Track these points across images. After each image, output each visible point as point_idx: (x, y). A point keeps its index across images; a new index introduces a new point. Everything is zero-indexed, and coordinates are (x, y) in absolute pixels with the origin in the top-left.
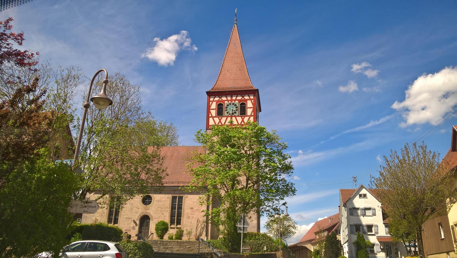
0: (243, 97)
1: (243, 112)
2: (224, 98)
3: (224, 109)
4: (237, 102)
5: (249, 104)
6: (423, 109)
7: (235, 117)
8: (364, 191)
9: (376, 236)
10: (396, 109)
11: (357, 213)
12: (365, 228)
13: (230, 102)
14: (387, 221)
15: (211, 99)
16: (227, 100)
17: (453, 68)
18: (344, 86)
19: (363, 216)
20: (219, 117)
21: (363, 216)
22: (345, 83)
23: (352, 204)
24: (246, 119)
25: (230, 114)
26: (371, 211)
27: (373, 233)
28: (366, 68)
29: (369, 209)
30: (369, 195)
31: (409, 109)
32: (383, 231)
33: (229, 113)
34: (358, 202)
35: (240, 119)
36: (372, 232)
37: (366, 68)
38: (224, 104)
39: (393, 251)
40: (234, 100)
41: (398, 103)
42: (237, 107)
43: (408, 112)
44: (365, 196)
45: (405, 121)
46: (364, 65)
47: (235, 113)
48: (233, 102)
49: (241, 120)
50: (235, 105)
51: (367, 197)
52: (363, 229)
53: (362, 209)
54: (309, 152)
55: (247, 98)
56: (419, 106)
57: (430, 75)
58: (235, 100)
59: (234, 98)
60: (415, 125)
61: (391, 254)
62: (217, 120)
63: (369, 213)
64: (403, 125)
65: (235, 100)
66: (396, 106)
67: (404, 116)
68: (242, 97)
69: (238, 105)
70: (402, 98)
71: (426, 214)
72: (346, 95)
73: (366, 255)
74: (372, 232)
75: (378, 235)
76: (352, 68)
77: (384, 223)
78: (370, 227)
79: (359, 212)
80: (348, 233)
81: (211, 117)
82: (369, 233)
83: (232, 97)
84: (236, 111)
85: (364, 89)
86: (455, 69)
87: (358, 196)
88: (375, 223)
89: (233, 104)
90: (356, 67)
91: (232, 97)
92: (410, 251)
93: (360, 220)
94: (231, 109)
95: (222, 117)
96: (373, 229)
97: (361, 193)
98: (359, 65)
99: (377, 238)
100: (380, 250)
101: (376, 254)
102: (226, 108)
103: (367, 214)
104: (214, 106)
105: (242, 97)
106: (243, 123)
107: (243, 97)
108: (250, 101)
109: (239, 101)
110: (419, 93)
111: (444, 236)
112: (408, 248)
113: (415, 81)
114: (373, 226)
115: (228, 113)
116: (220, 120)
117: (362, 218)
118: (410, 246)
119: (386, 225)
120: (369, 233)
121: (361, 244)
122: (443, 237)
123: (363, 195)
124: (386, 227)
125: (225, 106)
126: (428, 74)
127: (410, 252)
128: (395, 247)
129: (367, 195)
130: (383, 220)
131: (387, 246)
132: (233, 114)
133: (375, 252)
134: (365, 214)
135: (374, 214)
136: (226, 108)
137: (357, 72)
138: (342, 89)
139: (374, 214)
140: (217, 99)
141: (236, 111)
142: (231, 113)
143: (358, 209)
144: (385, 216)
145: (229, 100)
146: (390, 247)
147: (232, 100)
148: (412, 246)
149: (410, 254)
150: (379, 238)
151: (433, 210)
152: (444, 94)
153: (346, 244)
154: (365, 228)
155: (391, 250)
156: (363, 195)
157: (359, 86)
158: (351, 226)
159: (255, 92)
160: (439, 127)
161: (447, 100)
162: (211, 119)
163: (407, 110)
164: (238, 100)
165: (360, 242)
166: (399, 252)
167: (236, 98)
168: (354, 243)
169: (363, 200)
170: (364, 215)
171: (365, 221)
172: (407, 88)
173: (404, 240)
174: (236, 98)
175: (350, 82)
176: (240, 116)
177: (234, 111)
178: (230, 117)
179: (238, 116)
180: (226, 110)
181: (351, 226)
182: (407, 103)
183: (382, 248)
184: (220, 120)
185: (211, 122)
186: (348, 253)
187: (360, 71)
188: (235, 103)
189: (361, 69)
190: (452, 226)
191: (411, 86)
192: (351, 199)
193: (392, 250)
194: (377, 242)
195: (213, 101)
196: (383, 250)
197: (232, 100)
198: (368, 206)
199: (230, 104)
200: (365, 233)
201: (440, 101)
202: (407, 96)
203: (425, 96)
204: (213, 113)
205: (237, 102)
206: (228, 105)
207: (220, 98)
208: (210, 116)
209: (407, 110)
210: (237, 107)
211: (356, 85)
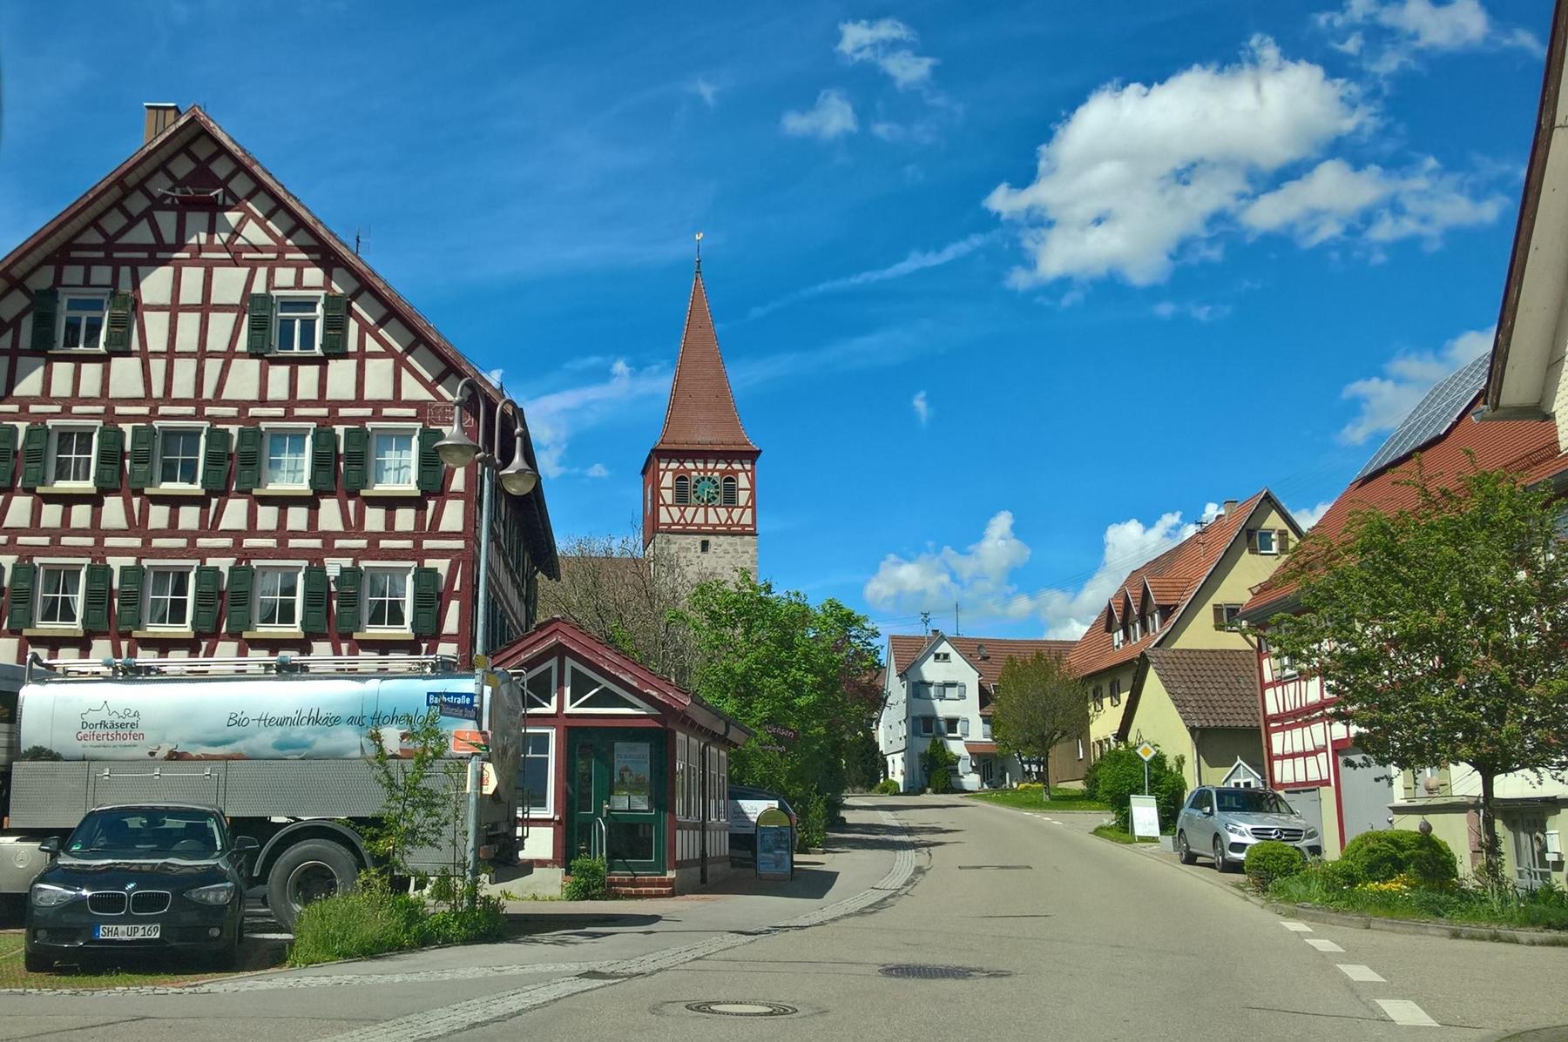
0: (730, 464)
1: (730, 500)
2: (690, 466)
3: (690, 489)
4: (716, 474)
5: (743, 481)
6: (1098, 221)
7: (715, 507)
8: (944, 648)
9: (962, 742)
10: (998, 214)
11: (928, 692)
12: (943, 725)
13: (702, 473)
14: (989, 710)
15: (663, 466)
16: (696, 469)
17: (1220, 70)
18: (803, 112)
19: (941, 700)
20: (679, 507)
21: (941, 700)
22: (807, 100)
23: (920, 674)
24: (736, 513)
25: (703, 501)
26: (957, 688)
27: (958, 734)
28: (893, 46)
29: (953, 685)
30: (954, 655)
31: (1051, 215)
32: (977, 731)
33: (701, 499)
34: (932, 671)
35: (723, 512)
36: (956, 732)
37: (893, 46)
38: (690, 478)
39: (996, 771)
40: (710, 470)
41: (1014, 190)
42: (717, 487)
43: (1043, 232)
44: (946, 656)
45: (1030, 264)
46: (887, 30)
47: (714, 498)
48: (709, 474)
49: (727, 515)
50: (714, 482)
51: (951, 660)
52: (938, 727)
53: (939, 685)
54: (655, 368)
55: (737, 466)
56: (1084, 210)
57: (1134, 88)
58: (714, 470)
59: (710, 466)
60: (1063, 283)
61: (991, 777)
62: (675, 512)
63: (951, 692)
64: (1020, 279)
65: (714, 470)
66: (1002, 200)
67: (1028, 244)
68: (726, 465)
69: (719, 483)
70: (1025, 177)
71: (1056, 737)
72: (810, 147)
73: (946, 779)
74: (956, 732)
75: (968, 739)
76: (838, 37)
77: (981, 716)
78: (952, 723)
79: (932, 690)
80: (907, 732)
81: (662, 505)
82: (950, 735)
83: (706, 463)
84: (716, 496)
85: (881, 129)
86: (1226, 74)
87: (932, 657)
88: (962, 715)
89: (709, 479)
90: (855, 36)
91: (706, 463)
92: (1030, 772)
93: (933, 709)
94: (706, 490)
95: (686, 507)
96: (958, 725)
97: (937, 651)
98: (870, 27)
99: (966, 745)
100: (970, 769)
101: (962, 777)
102: (695, 487)
103: (947, 696)
104: (668, 480)
105: (726, 465)
106: (730, 522)
107: (730, 464)
108: (744, 474)
109: (722, 472)
110: (1094, 158)
111: (1083, 755)
112: (1026, 767)
113: (1081, 111)
114: (958, 719)
115: (698, 498)
116: (682, 513)
117: (936, 702)
118: (1029, 763)
119: (986, 719)
120: (950, 735)
121: (939, 759)
122: (1081, 757)
123: (942, 656)
124: (984, 722)
125: (693, 482)
126: (1125, 84)
127: (1029, 775)
128: (999, 765)
129: (951, 655)
130: (980, 709)
131: (984, 761)
132: (709, 501)
133: (961, 773)
134: (944, 696)
135: (962, 697)
136: (695, 487)
137: (858, 57)
138: (795, 123)
139: (962, 697)
140: (674, 465)
141: (716, 496)
142: (705, 499)
143: (931, 684)
144: (985, 698)
145: (701, 470)
146: (991, 763)
147: (705, 470)
148: (1034, 763)
149: (1029, 778)
150: (969, 745)
151: (1064, 733)
152: (1180, 167)
153: (898, 757)
154: (943, 725)
155: (991, 770)
156: (942, 656)
157: (863, 114)
158: (915, 719)
159: (752, 456)
160: (1153, 293)
161: (1190, 193)
162: (662, 509)
163: (1040, 221)
164: (718, 471)
165: (936, 755)
166: (1008, 774)
167: (715, 466)
168: (923, 756)
169: (942, 665)
170: (942, 697)
171: (943, 709)
172: (1047, 136)
173: (1019, 753)
174: (715, 466)
175: (826, 96)
176: (723, 507)
177: (711, 496)
178: (702, 506)
179: (720, 506)
180: (695, 492)
181: (915, 719)
182: (1042, 193)
183: (974, 764)
184: (682, 513)
185: (664, 517)
186: (903, 773)
187: (867, 54)
188: (713, 477)
189: (874, 46)
190: (1093, 743)
191: (1065, 129)
192: (916, 664)
193: (993, 770)
194: (965, 753)
195: (666, 470)
196: (975, 770)
197: (705, 470)
198: (950, 679)
199: (703, 479)
200: (941, 734)
201: (1163, 191)
202: (1042, 165)
203: (1108, 171)
204: (668, 496)
205: (716, 474)
206: (698, 481)
207: (682, 463)
208: (661, 502)
209: (1040, 221)
210: (717, 487)
211: (849, 109)
